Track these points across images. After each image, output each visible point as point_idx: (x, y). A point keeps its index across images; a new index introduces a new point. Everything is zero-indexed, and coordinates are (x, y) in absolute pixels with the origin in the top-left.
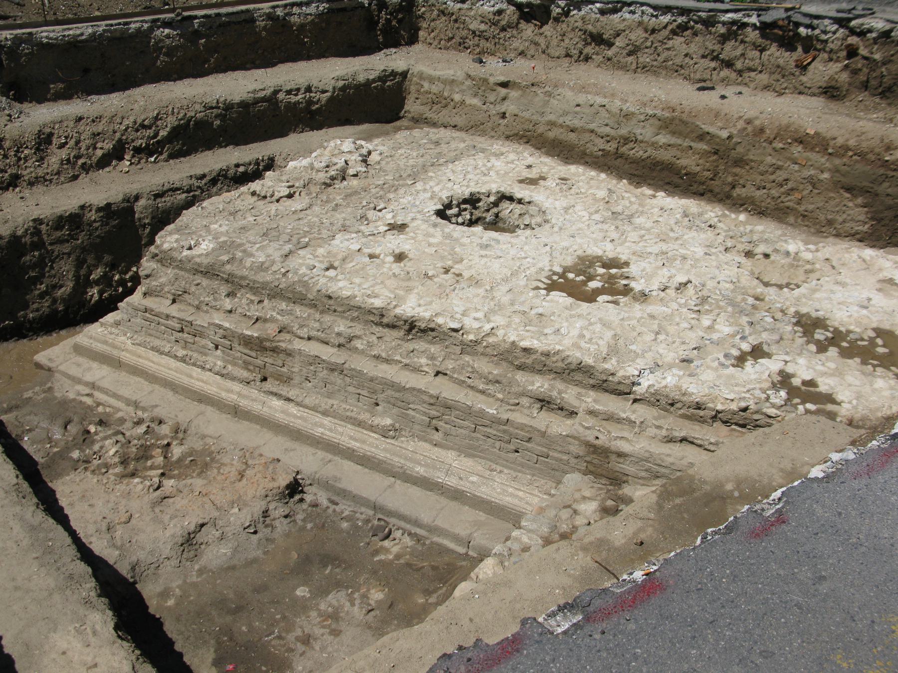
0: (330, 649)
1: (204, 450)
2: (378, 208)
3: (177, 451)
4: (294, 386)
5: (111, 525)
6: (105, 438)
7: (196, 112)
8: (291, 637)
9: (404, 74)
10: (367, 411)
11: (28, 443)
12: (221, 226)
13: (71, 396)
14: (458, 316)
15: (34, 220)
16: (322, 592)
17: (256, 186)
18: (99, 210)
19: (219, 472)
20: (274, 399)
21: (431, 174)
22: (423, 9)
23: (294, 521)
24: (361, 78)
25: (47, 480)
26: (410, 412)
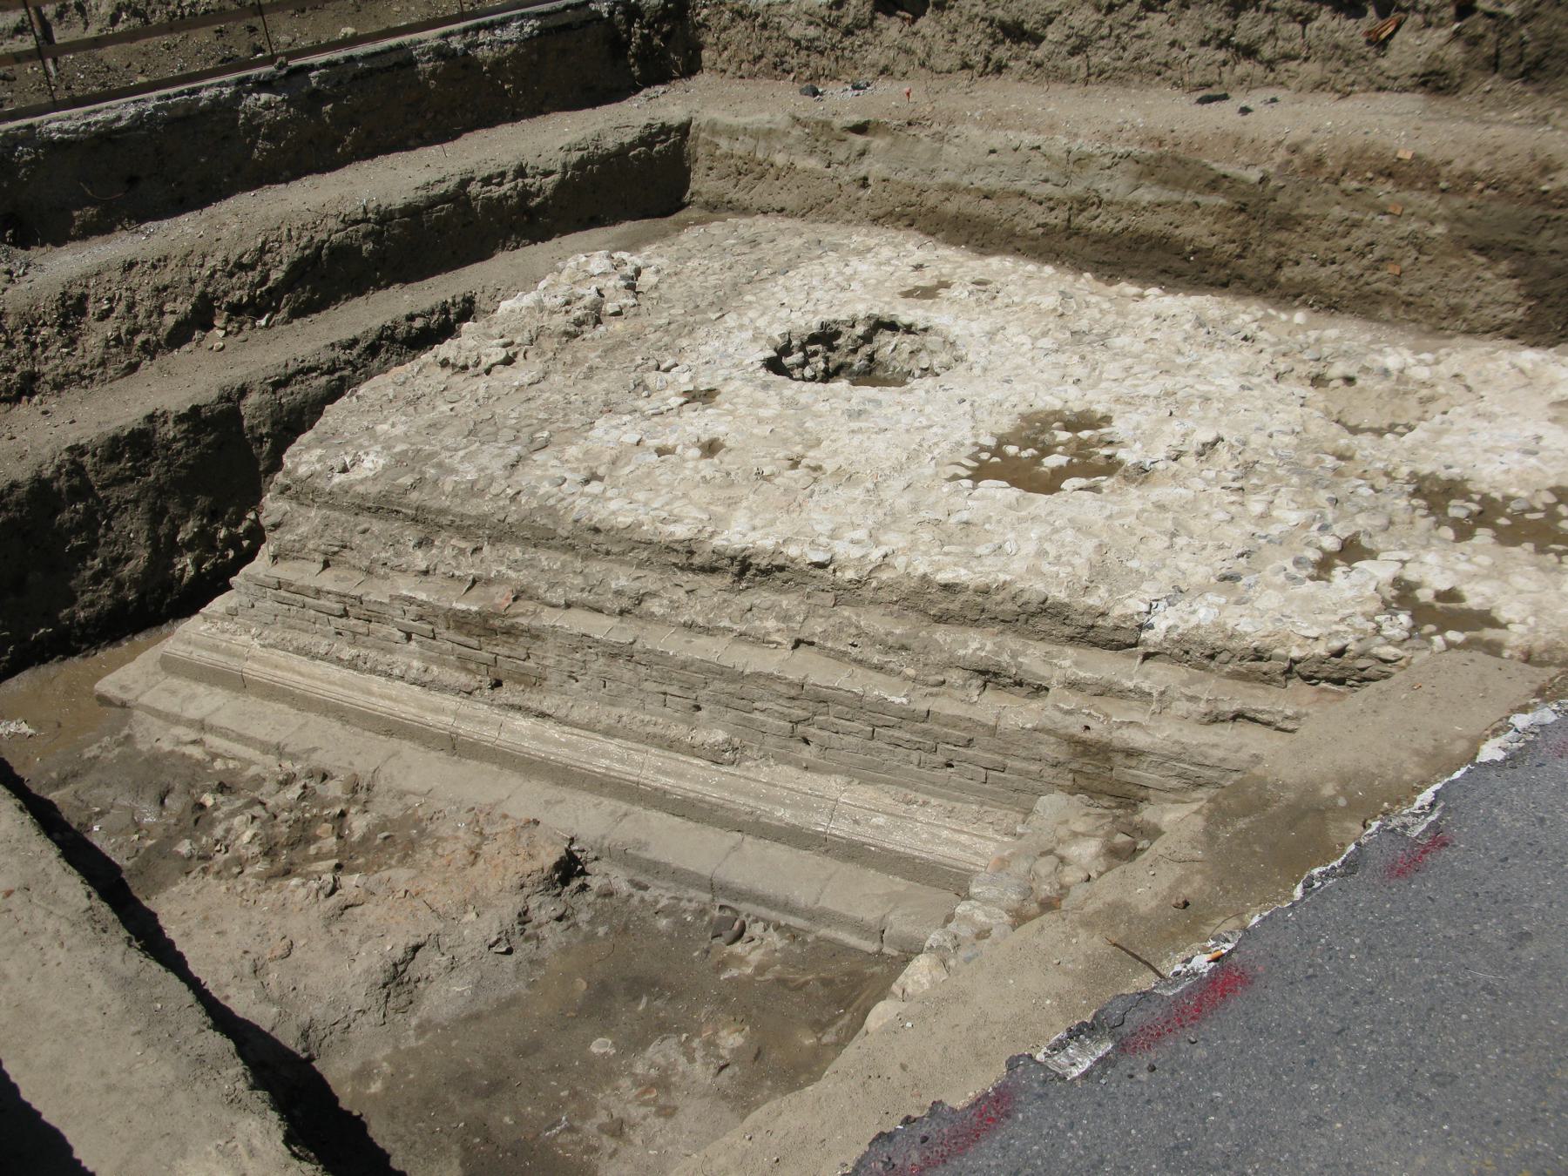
0: (660, 1141)
1: (405, 817)
2: (663, 367)
3: (358, 824)
4: (549, 691)
5: (259, 963)
6: (233, 814)
7: (331, 232)
8: (590, 1127)
9: (684, 129)
10: (683, 721)
11: (101, 836)
12: (394, 426)
13: (166, 746)
14: (823, 540)
15: (71, 449)
16: (636, 1043)
17: (446, 349)
18: (180, 419)
19: (435, 853)
20: (518, 716)
21: (748, 298)
22: (705, 12)
23: (575, 924)
24: (610, 143)
25: (140, 896)
26: (757, 715)
